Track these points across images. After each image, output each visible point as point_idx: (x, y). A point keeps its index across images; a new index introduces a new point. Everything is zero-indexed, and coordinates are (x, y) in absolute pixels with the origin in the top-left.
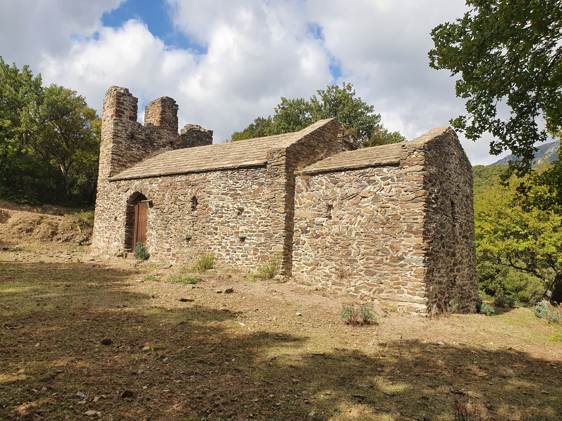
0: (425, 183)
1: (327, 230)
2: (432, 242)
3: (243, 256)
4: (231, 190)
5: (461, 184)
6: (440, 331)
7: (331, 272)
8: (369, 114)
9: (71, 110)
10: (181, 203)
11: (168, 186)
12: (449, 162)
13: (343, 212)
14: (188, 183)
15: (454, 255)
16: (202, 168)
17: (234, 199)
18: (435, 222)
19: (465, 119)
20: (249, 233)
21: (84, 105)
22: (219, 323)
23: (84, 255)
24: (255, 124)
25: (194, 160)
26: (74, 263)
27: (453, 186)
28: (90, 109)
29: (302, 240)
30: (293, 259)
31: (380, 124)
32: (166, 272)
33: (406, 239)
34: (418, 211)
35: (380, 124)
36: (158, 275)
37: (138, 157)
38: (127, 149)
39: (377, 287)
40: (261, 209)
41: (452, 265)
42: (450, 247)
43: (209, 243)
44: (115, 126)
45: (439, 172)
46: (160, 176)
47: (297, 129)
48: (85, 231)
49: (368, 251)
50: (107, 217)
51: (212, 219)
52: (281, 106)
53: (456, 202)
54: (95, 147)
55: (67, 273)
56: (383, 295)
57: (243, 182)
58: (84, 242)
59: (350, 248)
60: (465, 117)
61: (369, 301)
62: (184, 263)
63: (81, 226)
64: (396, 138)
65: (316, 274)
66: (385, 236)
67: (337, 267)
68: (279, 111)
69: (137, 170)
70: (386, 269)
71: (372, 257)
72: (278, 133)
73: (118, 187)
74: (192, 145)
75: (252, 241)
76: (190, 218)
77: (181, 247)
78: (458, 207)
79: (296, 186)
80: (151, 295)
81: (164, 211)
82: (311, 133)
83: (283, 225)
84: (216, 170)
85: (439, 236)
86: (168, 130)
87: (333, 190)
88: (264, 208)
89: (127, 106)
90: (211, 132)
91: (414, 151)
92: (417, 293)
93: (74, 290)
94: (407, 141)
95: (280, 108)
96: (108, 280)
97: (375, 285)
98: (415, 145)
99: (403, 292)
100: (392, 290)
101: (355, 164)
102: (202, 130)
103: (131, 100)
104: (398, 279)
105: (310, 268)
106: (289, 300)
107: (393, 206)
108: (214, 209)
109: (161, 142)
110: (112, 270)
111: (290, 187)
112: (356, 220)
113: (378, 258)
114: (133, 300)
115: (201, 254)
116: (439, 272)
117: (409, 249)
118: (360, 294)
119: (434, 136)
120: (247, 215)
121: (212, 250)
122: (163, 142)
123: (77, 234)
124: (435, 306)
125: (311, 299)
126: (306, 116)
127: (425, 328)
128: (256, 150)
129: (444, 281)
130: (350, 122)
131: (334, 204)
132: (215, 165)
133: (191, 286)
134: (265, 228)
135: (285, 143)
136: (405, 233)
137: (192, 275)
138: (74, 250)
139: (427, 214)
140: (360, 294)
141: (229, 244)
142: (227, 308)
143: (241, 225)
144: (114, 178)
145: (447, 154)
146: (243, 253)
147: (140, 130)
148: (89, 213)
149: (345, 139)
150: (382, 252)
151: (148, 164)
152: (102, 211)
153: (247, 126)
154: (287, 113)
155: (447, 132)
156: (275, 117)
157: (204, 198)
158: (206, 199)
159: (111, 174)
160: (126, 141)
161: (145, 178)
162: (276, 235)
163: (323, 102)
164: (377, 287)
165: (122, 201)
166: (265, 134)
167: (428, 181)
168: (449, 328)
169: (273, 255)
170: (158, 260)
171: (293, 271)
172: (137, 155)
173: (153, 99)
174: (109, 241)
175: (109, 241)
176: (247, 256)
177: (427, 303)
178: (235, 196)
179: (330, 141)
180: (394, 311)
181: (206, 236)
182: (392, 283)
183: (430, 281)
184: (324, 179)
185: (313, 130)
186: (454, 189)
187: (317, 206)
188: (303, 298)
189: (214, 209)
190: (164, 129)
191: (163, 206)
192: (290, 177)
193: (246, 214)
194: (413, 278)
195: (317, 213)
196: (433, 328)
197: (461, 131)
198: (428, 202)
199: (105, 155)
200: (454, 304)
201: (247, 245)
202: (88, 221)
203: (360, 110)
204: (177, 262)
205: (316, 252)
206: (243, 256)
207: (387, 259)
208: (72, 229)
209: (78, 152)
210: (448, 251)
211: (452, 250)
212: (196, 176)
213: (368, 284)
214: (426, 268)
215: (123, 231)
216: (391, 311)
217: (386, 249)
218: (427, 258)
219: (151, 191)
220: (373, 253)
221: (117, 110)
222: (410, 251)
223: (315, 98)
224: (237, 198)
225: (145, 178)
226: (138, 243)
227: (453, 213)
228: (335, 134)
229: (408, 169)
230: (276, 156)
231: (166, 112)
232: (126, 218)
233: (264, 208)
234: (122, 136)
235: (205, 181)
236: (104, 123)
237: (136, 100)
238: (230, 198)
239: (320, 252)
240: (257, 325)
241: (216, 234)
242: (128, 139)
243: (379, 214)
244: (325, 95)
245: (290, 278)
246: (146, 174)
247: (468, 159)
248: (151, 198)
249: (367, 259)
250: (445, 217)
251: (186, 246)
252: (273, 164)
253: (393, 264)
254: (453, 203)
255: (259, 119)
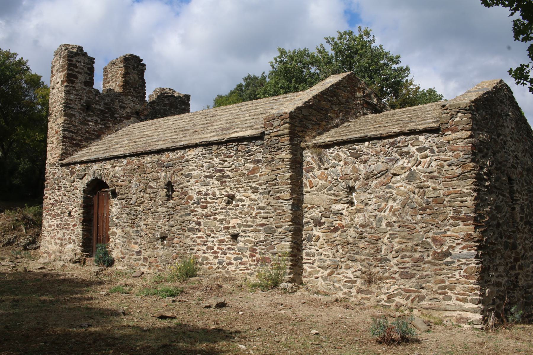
0: (473, 153)
1: (348, 221)
2: (485, 231)
3: (236, 259)
4: (217, 171)
5: (520, 154)
6: (501, 347)
7: (356, 277)
8: (395, 66)
9: (11, 78)
10: (152, 191)
11: (135, 169)
12: (502, 126)
13: (368, 196)
14: (160, 164)
15: (514, 247)
16: (179, 144)
17: (222, 183)
18: (489, 205)
19: (528, 69)
20: (243, 228)
21: (26, 70)
22: (211, 345)
23: (30, 261)
24: (244, 84)
25: (168, 133)
26: (20, 272)
27: (509, 157)
28: (33, 75)
29: (315, 235)
30: (304, 261)
31: (409, 78)
32: (136, 281)
33: (452, 228)
34: (466, 191)
35: (409, 78)
36: (127, 285)
37: (96, 133)
38: (81, 123)
39: (417, 294)
40: (258, 196)
41: (512, 260)
42: (509, 237)
43: (191, 243)
44: (66, 94)
45: (491, 138)
46: (125, 156)
47: (300, 88)
48: (31, 232)
49: (403, 246)
50: (59, 212)
51: (193, 211)
52: (279, 60)
53: (514, 177)
54: (40, 123)
55: (12, 285)
56: (425, 303)
57: (234, 161)
58: (30, 246)
59: (380, 243)
60: (527, 66)
61: (407, 312)
62: (159, 270)
63: (25, 224)
64: (431, 96)
65: (336, 279)
66: (424, 225)
67: (364, 269)
68: (276, 65)
69: (95, 150)
70: (428, 269)
71: (409, 254)
72: (275, 94)
73: (72, 173)
74: (164, 115)
75: (247, 238)
76: (165, 210)
77: (155, 249)
78: (517, 184)
79: (304, 163)
80: (120, 310)
81: (132, 202)
82: (321, 93)
83: (289, 216)
84: (196, 146)
85: (495, 223)
86: (132, 96)
87: (354, 167)
88: (262, 193)
89: (81, 68)
90: (188, 97)
91: (458, 112)
92: (469, 298)
93: (24, 306)
94: (446, 100)
95: (276, 61)
96: (65, 292)
97: (413, 291)
98: (459, 104)
99: (450, 298)
100: (437, 296)
101: (382, 132)
102: (176, 95)
103: (86, 61)
104: (443, 281)
105: (327, 272)
106: (301, 315)
107: (433, 185)
108: (195, 197)
109: (124, 112)
110: (68, 280)
111: (297, 165)
112: (386, 205)
113: (417, 255)
114: (98, 317)
115: (181, 257)
116: (496, 270)
117: (456, 241)
118: (394, 303)
119: (482, 92)
120: (240, 204)
121: (194, 252)
122: (127, 112)
123: (20, 236)
124: (492, 315)
125: (330, 313)
126: (312, 70)
127: (481, 344)
128: (248, 118)
129: (503, 282)
130: (371, 78)
131: (357, 184)
132: (196, 139)
133: (170, 299)
134: (264, 221)
135: (287, 107)
136: (451, 221)
137: (171, 286)
138: (19, 256)
139: (478, 194)
140: (394, 303)
141: (217, 244)
142: (220, 326)
143: (232, 218)
144: (66, 161)
145: (500, 116)
146: (235, 256)
147: (98, 99)
148: (36, 208)
149: (367, 99)
150: (422, 247)
151: (109, 142)
152: (53, 204)
153: (233, 87)
154: (286, 67)
155: (499, 86)
156: (271, 73)
157: (182, 183)
158: (185, 184)
159: (63, 156)
160: (81, 113)
161: (106, 159)
162: (280, 230)
163: (333, 53)
164: (417, 294)
165: (78, 191)
166: (259, 96)
167: (478, 151)
168: (511, 342)
169: (276, 257)
170: (126, 267)
171: (305, 277)
172: (94, 131)
173: (113, 58)
174: (62, 244)
175: (62, 244)
176: (241, 259)
177: (482, 312)
178: (223, 179)
179: (347, 101)
180: (440, 323)
181: (187, 233)
182: (436, 288)
183: (486, 282)
184: (342, 152)
185: (323, 88)
186: (511, 160)
187: (334, 188)
188: (319, 311)
189: (195, 197)
190: (128, 95)
191: (129, 195)
192: (295, 151)
193: (239, 203)
194: (463, 279)
195: (334, 198)
196: (491, 344)
197: (523, 84)
198: (479, 178)
199: (54, 132)
200: (517, 312)
201: (241, 245)
202: (34, 218)
203: (382, 62)
204: (149, 268)
205: (334, 251)
206: (236, 259)
207: (428, 256)
208: (15, 228)
209: (19, 130)
210: (506, 243)
211: (512, 241)
212: (171, 155)
213: (405, 290)
214: (480, 266)
215: (79, 230)
216: (436, 324)
217: (427, 242)
218: (480, 252)
219: (114, 176)
220: (409, 249)
221: (68, 74)
222: (458, 244)
223: (323, 48)
224: (225, 182)
225: (106, 159)
226: (99, 245)
227: (512, 192)
228: (353, 93)
229: (451, 136)
230: (276, 123)
231: (129, 74)
232: (83, 213)
233: (262, 193)
234: (76, 107)
235: (183, 160)
236: (52, 92)
237: (92, 61)
238: (216, 182)
239: (340, 251)
240: (261, 348)
241: (200, 231)
242: (83, 110)
243: (416, 196)
244: (336, 44)
245: (301, 286)
246: (107, 155)
247: (526, 120)
248: (114, 185)
249: (403, 257)
250: (501, 197)
251: (161, 247)
252: (272, 135)
253: (436, 261)
254: (510, 179)
255: (249, 77)
